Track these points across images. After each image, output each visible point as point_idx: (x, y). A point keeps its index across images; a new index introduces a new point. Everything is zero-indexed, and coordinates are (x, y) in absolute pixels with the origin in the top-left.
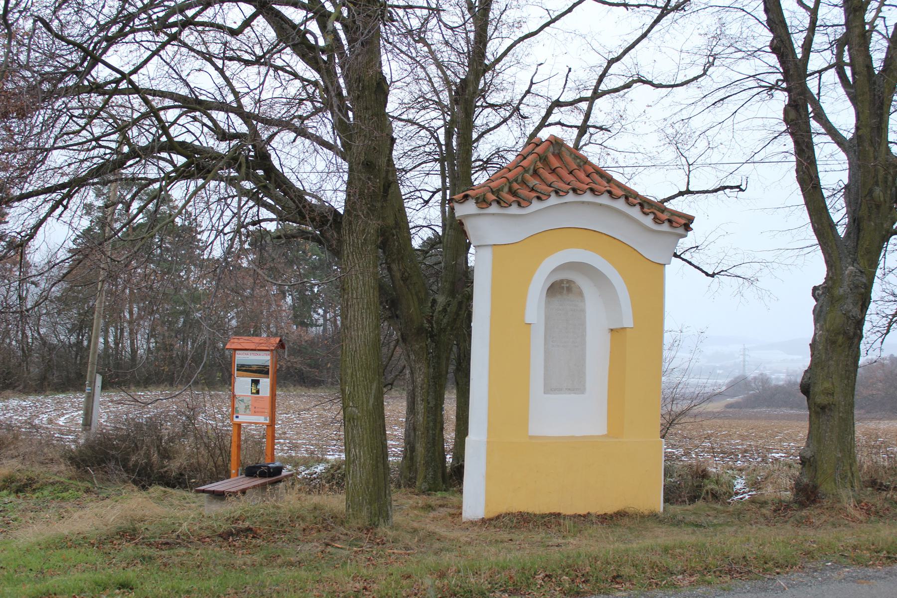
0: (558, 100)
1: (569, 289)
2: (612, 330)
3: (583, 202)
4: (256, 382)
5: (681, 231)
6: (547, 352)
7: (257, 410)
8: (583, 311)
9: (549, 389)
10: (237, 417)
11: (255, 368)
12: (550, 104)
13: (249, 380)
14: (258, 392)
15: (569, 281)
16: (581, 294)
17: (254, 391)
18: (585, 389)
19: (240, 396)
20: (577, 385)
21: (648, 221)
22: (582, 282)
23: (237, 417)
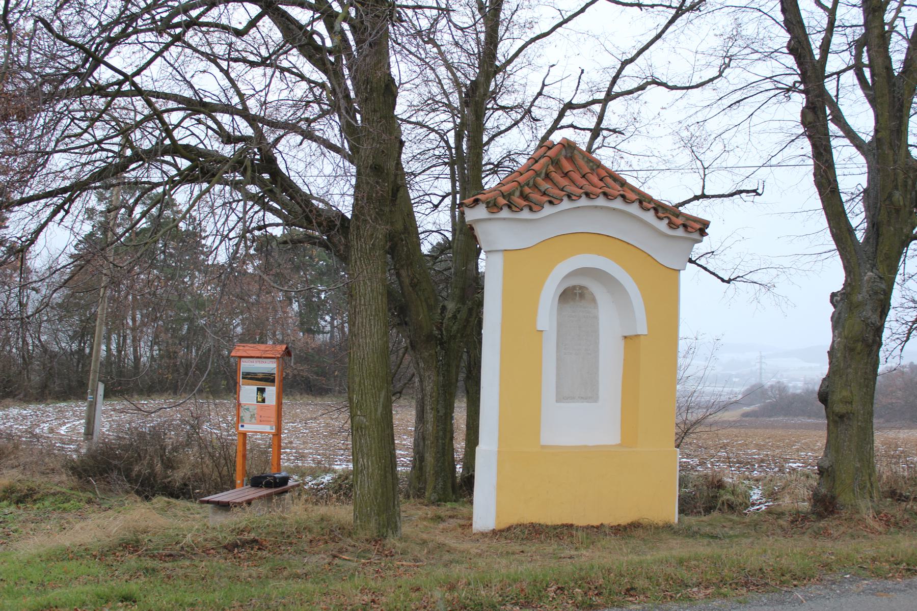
0: (570, 102)
1: (582, 296)
2: (625, 337)
3: (596, 207)
4: (261, 391)
5: (696, 236)
6: (559, 359)
7: (263, 419)
8: (596, 318)
9: (561, 397)
10: (242, 426)
11: (261, 376)
12: (562, 106)
13: (255, 388)
14: (263, 401)
15: (581, 287)
16: (594, 300)
17: (260, 400)
18: (598, 398)
19: (245, 405)
20: (587, 390)
21: (663, 226)
22: (595, 288)
23: (242, 426)
